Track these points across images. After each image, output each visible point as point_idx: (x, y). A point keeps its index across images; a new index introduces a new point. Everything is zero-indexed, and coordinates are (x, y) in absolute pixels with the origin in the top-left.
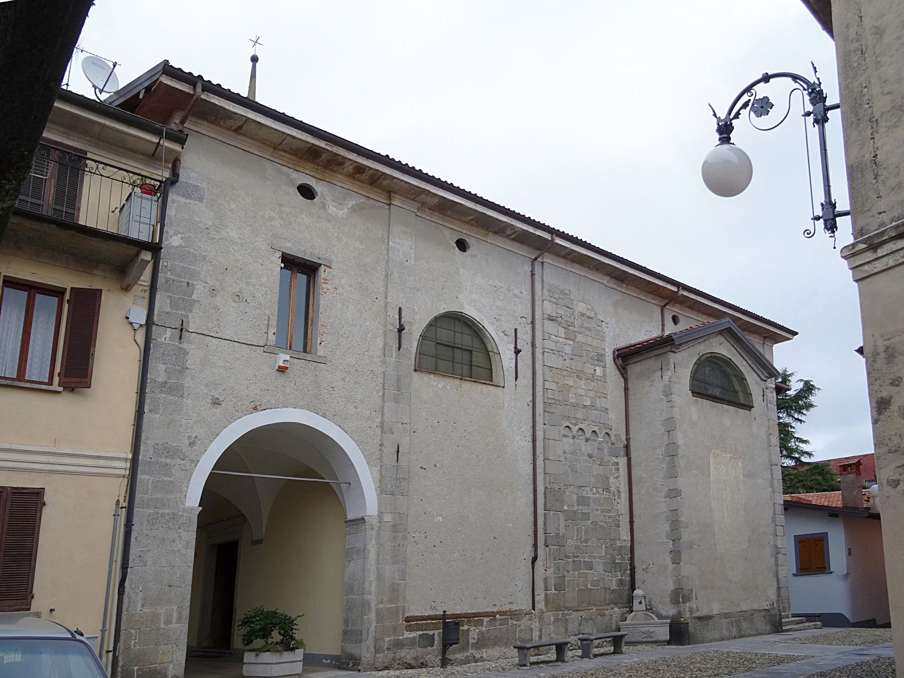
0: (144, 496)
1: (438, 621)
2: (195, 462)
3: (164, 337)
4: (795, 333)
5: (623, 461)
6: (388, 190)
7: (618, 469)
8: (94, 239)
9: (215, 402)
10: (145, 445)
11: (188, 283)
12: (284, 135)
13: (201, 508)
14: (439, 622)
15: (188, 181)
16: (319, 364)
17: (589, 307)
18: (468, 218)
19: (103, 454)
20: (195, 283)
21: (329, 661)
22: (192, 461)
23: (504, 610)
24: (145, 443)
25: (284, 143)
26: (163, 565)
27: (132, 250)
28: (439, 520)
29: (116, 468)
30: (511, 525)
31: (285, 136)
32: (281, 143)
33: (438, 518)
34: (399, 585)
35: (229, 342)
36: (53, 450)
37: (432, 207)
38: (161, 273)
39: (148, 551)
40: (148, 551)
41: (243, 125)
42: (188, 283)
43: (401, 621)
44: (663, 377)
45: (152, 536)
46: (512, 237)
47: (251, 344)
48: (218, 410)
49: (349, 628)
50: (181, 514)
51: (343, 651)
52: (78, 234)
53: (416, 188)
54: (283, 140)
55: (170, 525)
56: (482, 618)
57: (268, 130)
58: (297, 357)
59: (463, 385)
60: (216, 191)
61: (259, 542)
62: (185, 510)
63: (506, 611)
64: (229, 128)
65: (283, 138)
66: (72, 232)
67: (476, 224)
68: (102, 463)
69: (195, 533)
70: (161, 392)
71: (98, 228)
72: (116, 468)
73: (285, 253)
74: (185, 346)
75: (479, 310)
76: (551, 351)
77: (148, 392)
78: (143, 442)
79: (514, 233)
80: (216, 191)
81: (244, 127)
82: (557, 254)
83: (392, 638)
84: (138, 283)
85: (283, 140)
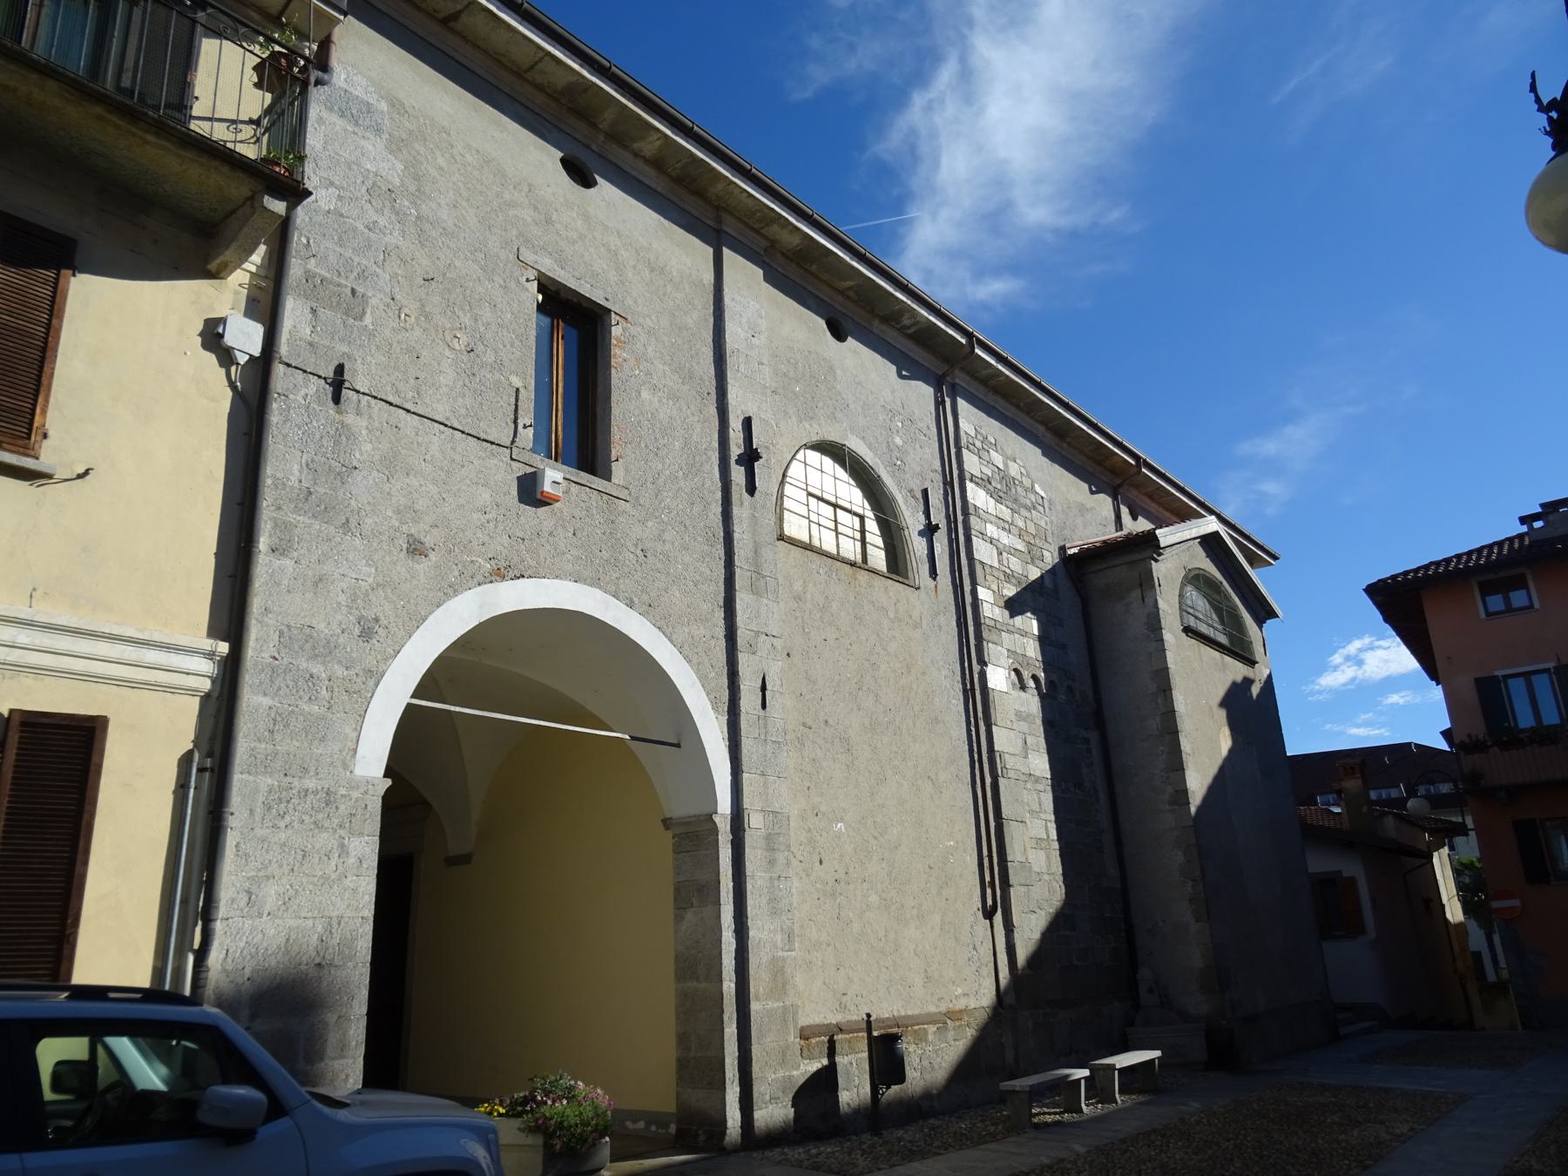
0: (258, 745)
1: (855, 1035)
2: (376, 676)
3: (303, 392)
4: (1275, 558)
5: (1093, 736)
6: (716, 204)
7: (1089, 751)
8: (150, 138)
9: (415, 549)
10: (259, 625)
11: (353, 291)
12: (540, 51)
13: (389, 782)
14: (857, 1037)
15: (351, 90)
16: (616, 500)
17: (1023, 471)
18: (844, 283)
19: (157, 637)
20: (370, 294)
21: (641, 1125)
22: (369, 672)
23: (957, 1008)
24: (261, 622)
25: (537, 67)
26: (303, 915)
27: (238, 188)
28: (841, 828)
29: (188, 674)
30: (952, 843)
31: (541, 54)
32: (532, 68)
33: (839, 826)
34: (784, 959)
35: (442, 427)
36: (24, 613)
37: (788, 251)
38: (295, 257)
39: (268, 878)
40: (268, 878)
41: (461, 12)
42: (353, 291)
43: (793, 1038)
44: (1146, 600)
45: (276, 843)
46: (910, 331)
47: (487, 438)
48: (422, 567)
49: (692, 1054)
50: (344, 793)
51: (680, 1104)
52: (114, 119)
53: (766, 211)
54: (536, 63)
55: (320, 816)
56: (926, 1026)
57: (511, 35)
58: (575, 480)
59: (859, 577)
60: (407, 124)
61: (465, 859)
62: (353, 785)
63: (961, 1011)
64: (432, 12)
65: (537, 59)
66: (99, 110)
67: (856, 298)
68: (152, 656)
69: (378, 838)
70: (297, 510)
71: (219, 41)
72: (188, 674)
73: (544, 274)
74: (350, 419)
75: (870, 447)
76: (981, 536)
77: (268, 506)
78: (257, 619)
79: (914, 324)
80: (407, 124)
81: (462, 16)
82: (973, 375)
83: (780, 1074)
84: (244, 266)
85: (536, 63)
